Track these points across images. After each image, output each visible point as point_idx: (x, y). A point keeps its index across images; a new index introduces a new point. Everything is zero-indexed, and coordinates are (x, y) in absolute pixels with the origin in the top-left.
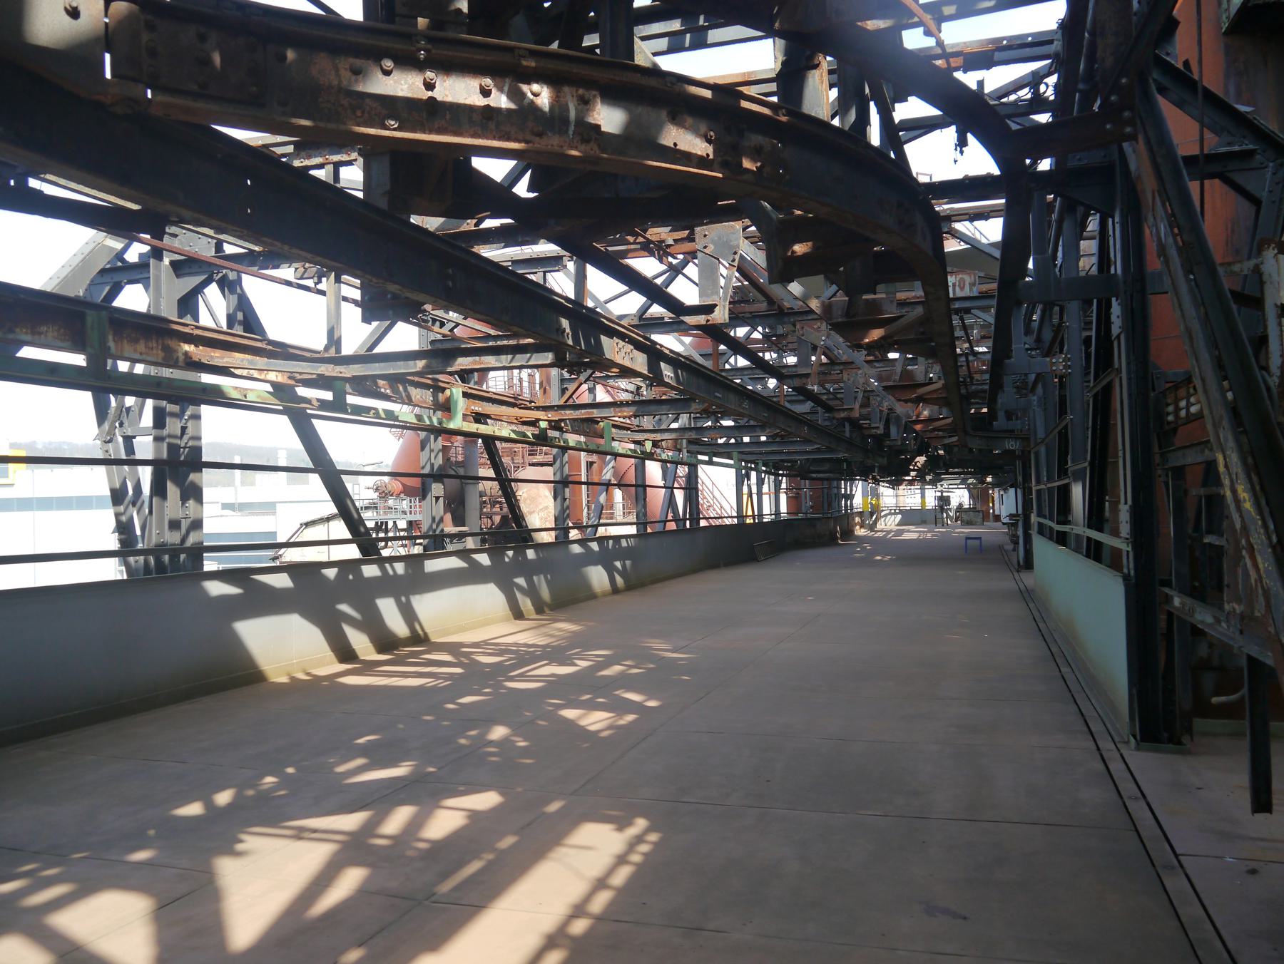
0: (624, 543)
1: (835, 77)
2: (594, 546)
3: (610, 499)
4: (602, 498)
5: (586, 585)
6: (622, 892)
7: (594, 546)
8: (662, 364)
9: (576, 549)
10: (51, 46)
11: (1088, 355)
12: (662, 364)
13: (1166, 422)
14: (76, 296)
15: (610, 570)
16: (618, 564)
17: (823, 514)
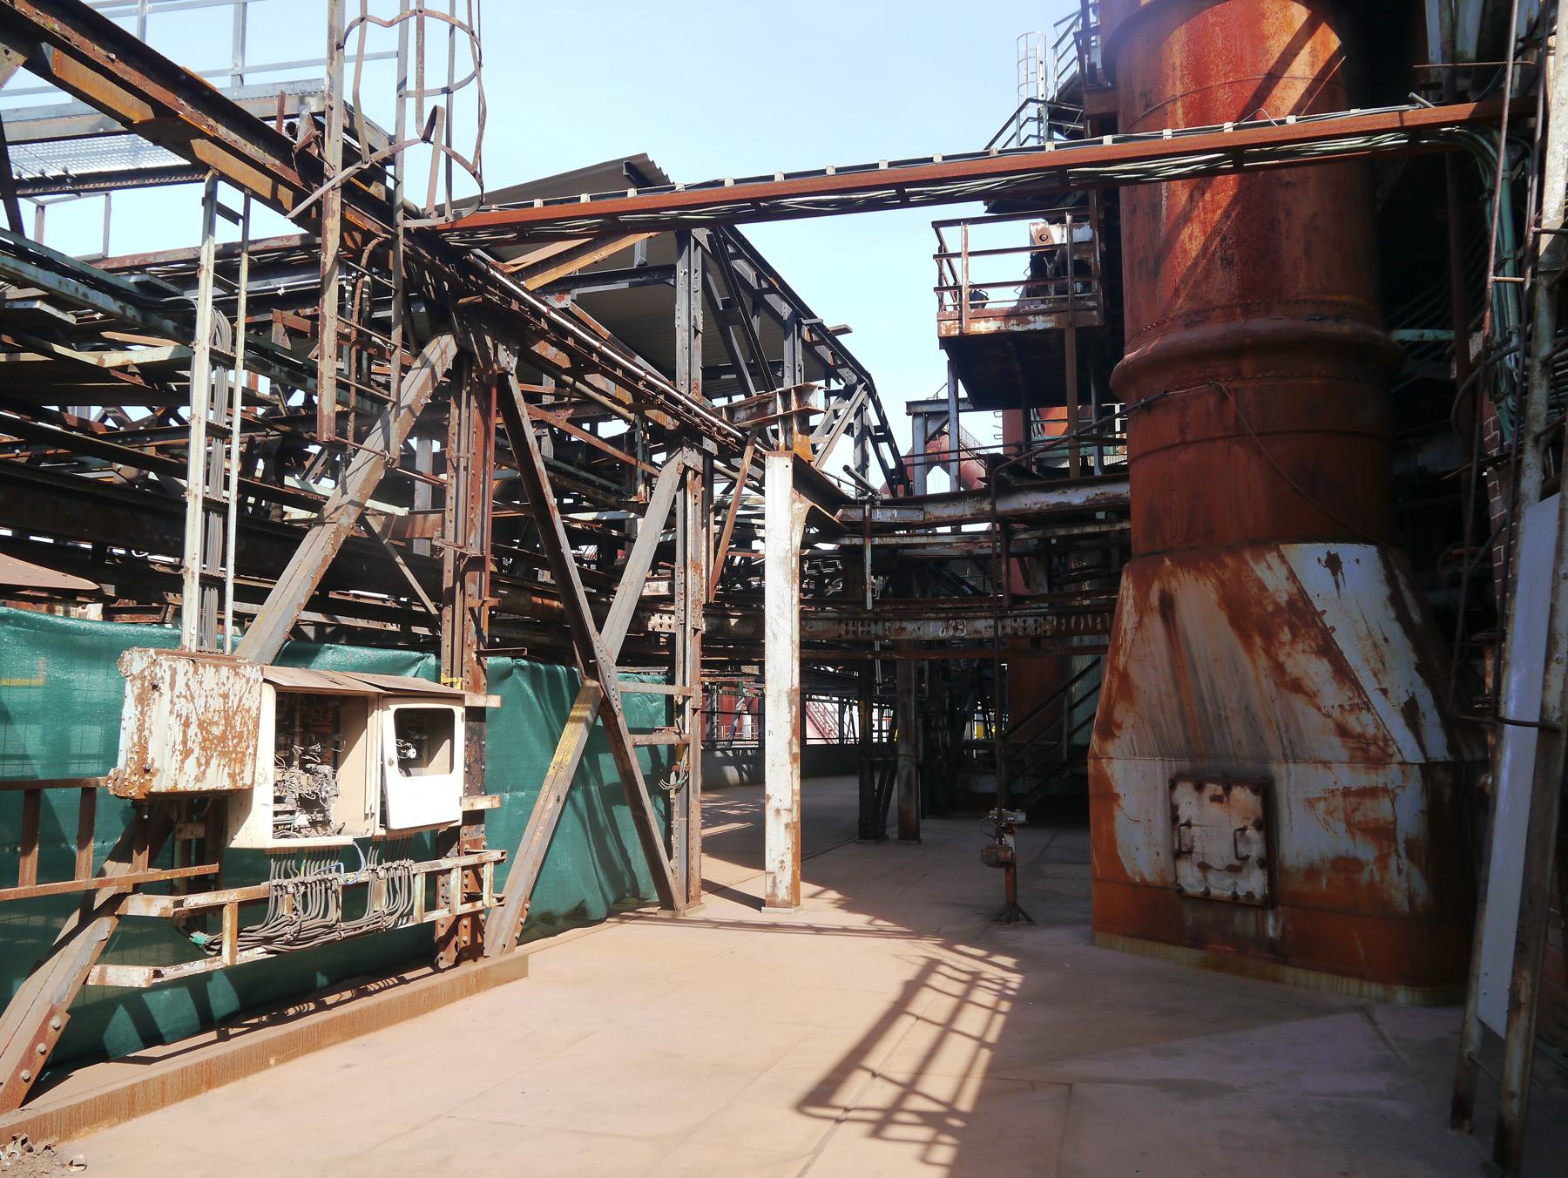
0: (749, 753)
1: (845, 793)
2: (730, 753)
3: (741, 722)
4: (736, 723)
5: (724, 776)
6: (1376, 152)
7: (730, 753)
8: (44, 45)
9: (719, 754)
10: (1177, 618)
11: (585, 830)
12: (44, 45)
13: (155, 980)
14: (123, 820)
15: (740, 770)
16: (745, 766)
17: (998, 612)
